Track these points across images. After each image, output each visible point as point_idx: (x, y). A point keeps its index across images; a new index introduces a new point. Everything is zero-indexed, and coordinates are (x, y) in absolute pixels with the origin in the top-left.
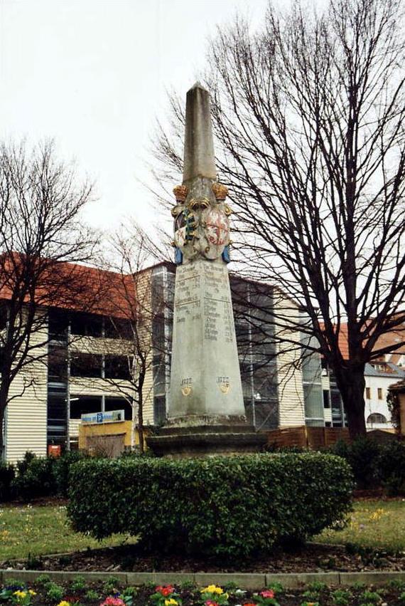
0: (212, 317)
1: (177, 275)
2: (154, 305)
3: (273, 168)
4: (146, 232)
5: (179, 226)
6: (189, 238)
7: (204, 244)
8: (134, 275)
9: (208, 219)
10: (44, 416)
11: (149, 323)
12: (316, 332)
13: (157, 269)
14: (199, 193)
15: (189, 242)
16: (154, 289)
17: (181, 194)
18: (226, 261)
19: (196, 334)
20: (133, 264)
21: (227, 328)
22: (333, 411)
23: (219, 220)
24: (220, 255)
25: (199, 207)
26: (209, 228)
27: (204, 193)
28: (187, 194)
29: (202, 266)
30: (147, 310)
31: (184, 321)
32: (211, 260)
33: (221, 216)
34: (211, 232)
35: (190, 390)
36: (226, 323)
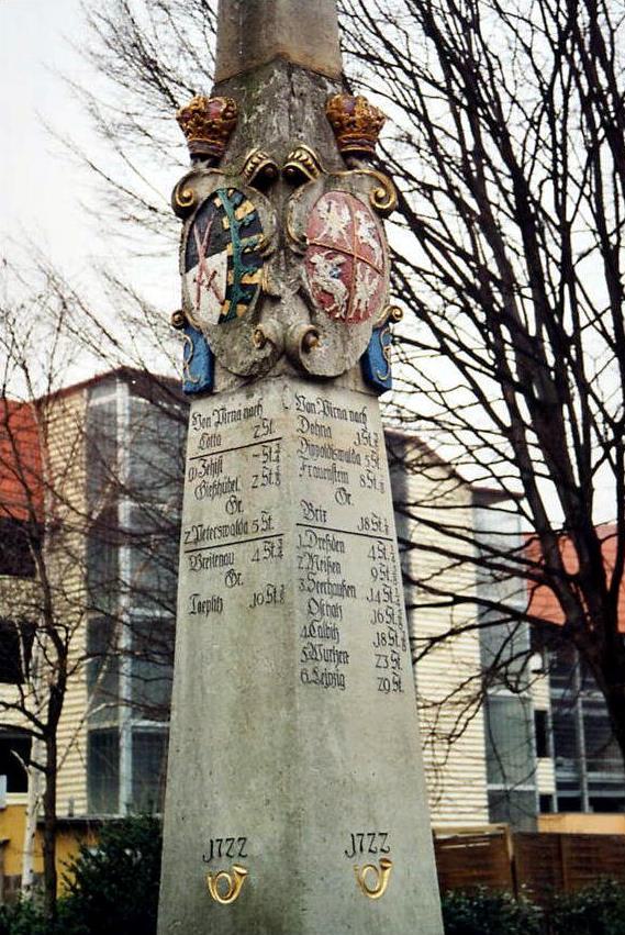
0: (327, 599)
1: (194, 434)
2: (91, 492)
3: (439, 110)
4: (73, 285)
5: (200, 249)
6: (238, 293)
7: (299, 322)
8: (39, 403)
11: (77, 543)
12: (546, 574)
13: (101, 389)
14: (279, 124)
15: (241, 308)
16: (95, 447)
17: (210, 130)
18: (375, 387)
19: (265, 667)
20: (37, 374)
21: (382, 639)
22: (558, 766)
23: (351, 229)
24: (353, 362)
25: (277, 180)
26: (317, 259)
27: (296, 126)
28: (232, 128)
29: (290, 400)
30: (74, 501)
31: (219, 610)
32: (324, 382)
33: (359, 215)
34: (323, 273)
35: (240, 882)
36: (378, 616)
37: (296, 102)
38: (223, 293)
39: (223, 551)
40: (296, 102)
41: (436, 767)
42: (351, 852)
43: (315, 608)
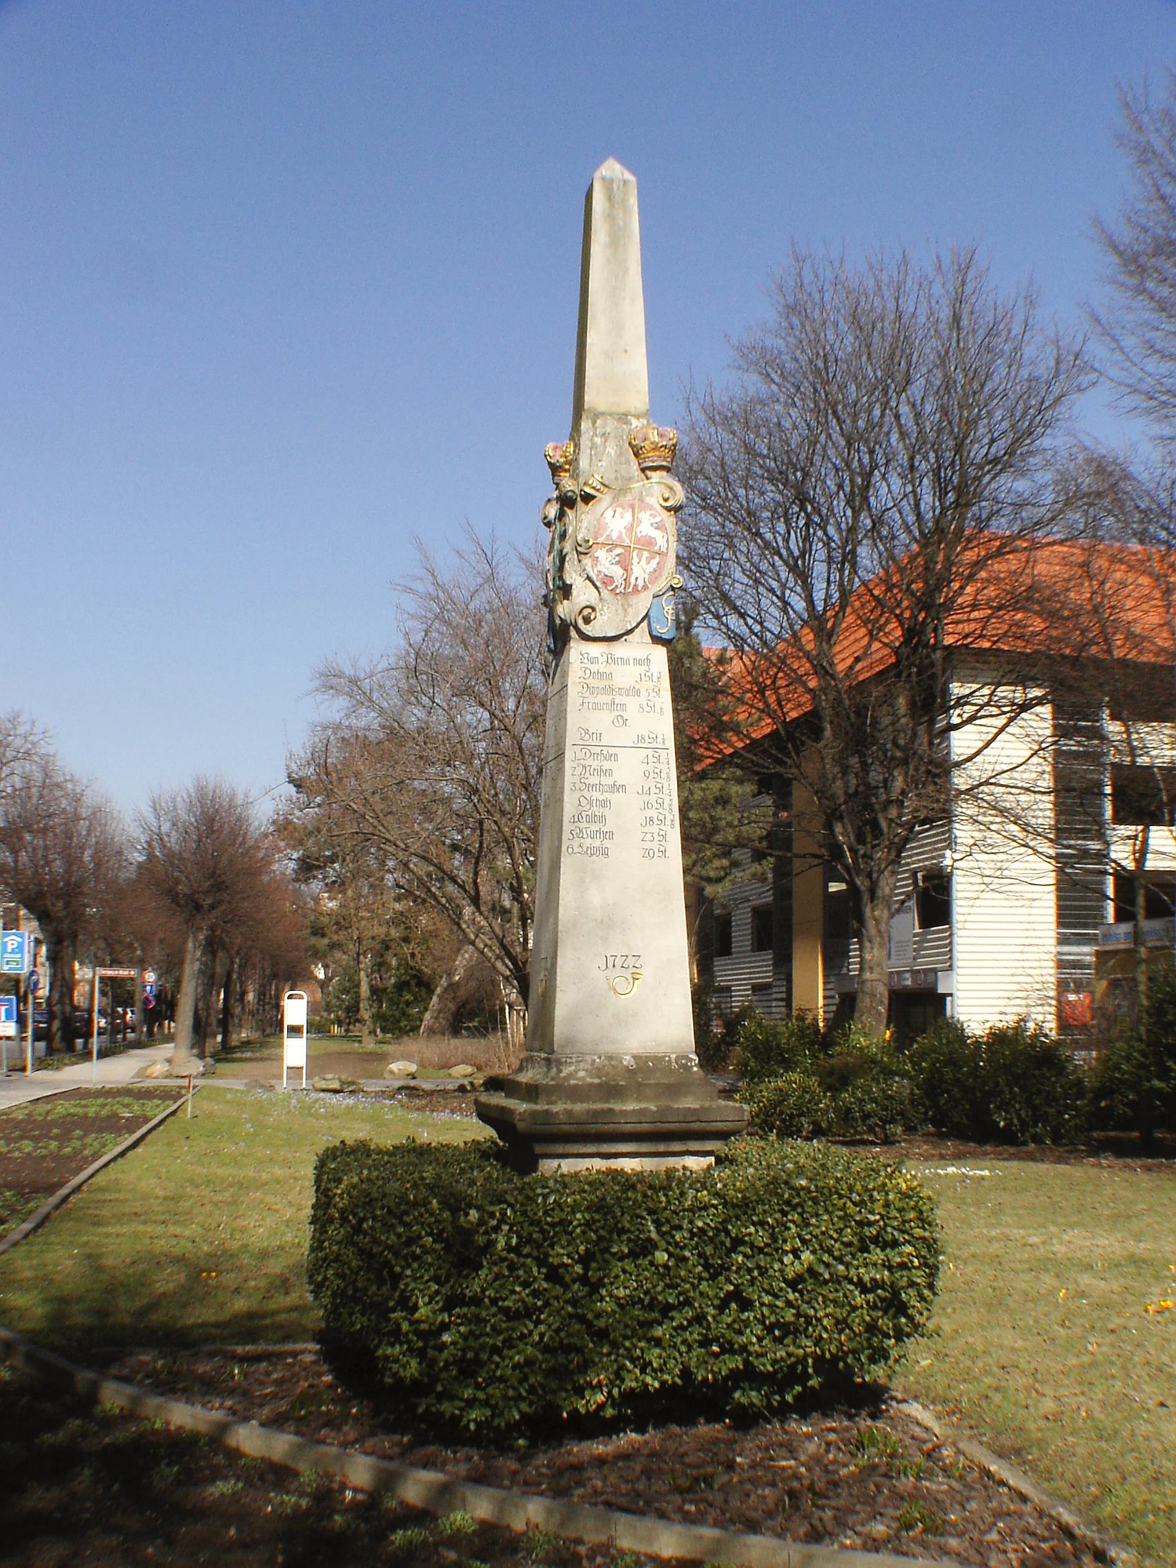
9: (599, 527)
37: (598, 440)
40: (598, 440)
41: (1128, 1058)
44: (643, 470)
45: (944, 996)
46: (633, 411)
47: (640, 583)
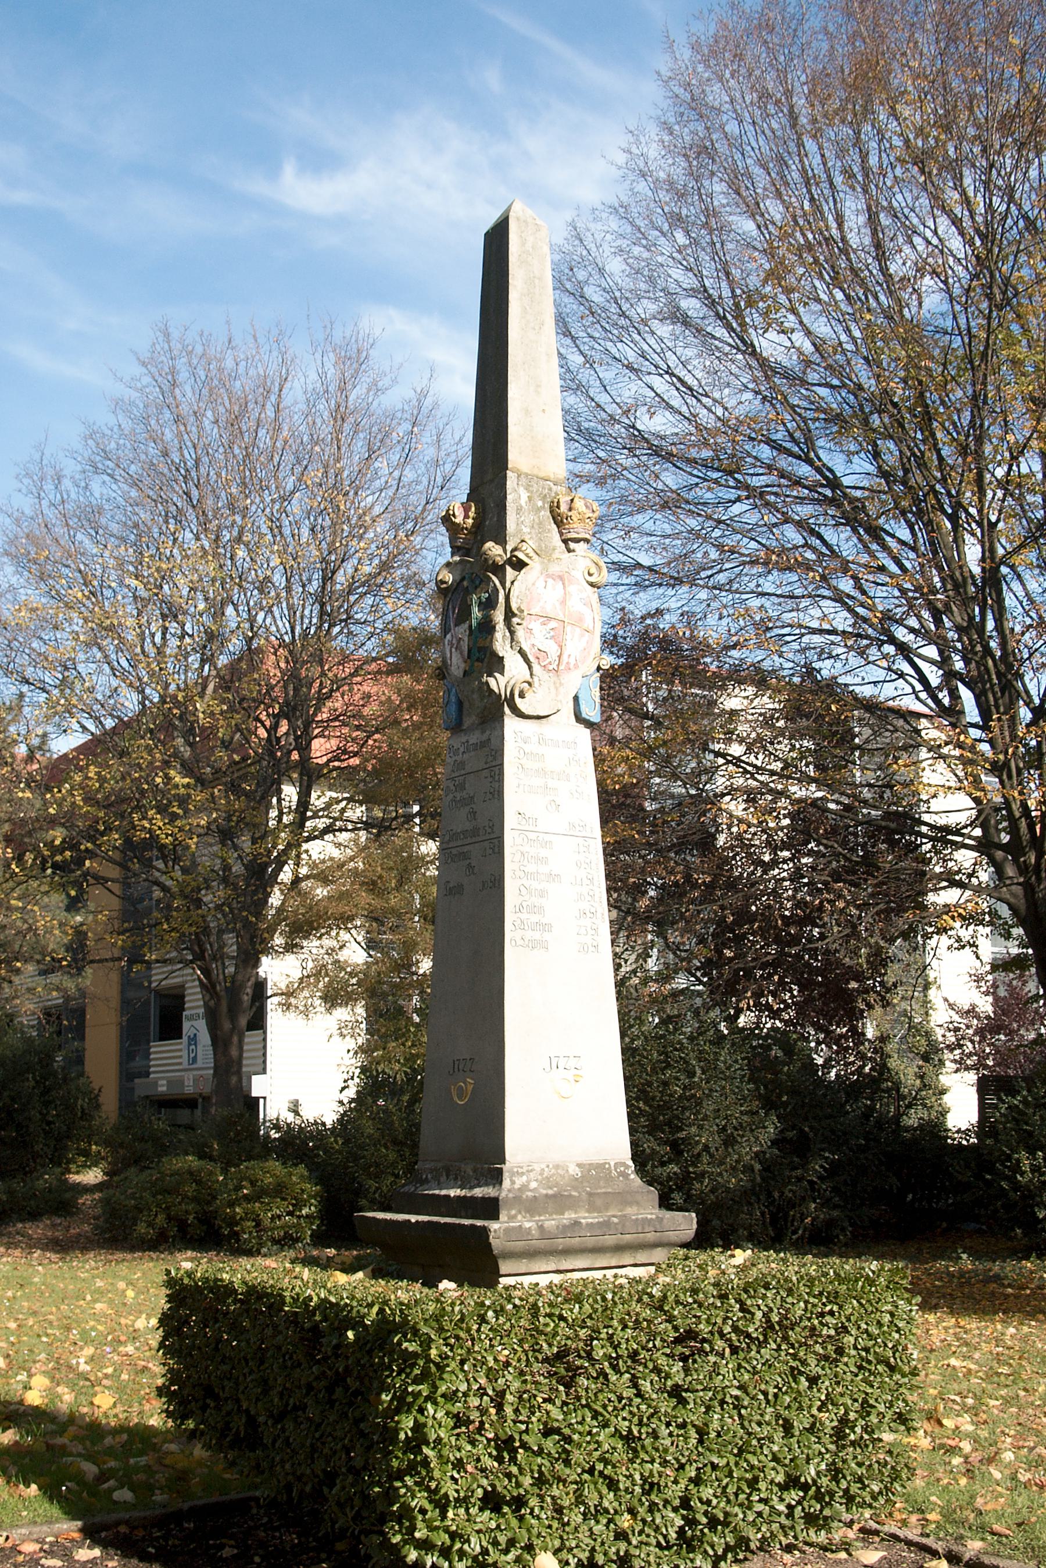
10: (197, 1000)
38: (466, 653)
39: (465, 849)
42: (548, 1068)
43: (524, 891)
44: (565, 541)
45: (257, 1099)
46: (552, 477)
47: (572, 661)
